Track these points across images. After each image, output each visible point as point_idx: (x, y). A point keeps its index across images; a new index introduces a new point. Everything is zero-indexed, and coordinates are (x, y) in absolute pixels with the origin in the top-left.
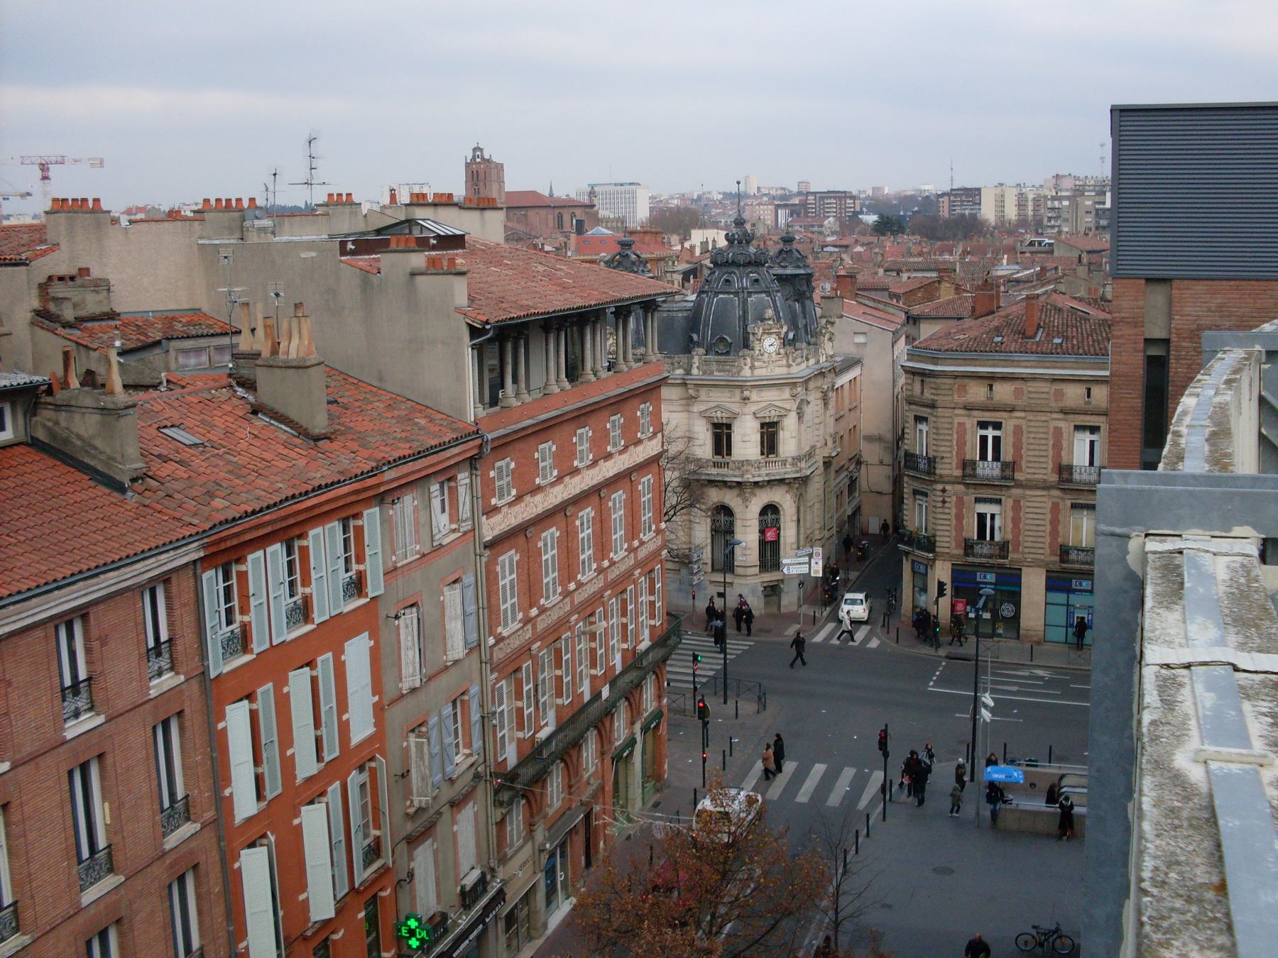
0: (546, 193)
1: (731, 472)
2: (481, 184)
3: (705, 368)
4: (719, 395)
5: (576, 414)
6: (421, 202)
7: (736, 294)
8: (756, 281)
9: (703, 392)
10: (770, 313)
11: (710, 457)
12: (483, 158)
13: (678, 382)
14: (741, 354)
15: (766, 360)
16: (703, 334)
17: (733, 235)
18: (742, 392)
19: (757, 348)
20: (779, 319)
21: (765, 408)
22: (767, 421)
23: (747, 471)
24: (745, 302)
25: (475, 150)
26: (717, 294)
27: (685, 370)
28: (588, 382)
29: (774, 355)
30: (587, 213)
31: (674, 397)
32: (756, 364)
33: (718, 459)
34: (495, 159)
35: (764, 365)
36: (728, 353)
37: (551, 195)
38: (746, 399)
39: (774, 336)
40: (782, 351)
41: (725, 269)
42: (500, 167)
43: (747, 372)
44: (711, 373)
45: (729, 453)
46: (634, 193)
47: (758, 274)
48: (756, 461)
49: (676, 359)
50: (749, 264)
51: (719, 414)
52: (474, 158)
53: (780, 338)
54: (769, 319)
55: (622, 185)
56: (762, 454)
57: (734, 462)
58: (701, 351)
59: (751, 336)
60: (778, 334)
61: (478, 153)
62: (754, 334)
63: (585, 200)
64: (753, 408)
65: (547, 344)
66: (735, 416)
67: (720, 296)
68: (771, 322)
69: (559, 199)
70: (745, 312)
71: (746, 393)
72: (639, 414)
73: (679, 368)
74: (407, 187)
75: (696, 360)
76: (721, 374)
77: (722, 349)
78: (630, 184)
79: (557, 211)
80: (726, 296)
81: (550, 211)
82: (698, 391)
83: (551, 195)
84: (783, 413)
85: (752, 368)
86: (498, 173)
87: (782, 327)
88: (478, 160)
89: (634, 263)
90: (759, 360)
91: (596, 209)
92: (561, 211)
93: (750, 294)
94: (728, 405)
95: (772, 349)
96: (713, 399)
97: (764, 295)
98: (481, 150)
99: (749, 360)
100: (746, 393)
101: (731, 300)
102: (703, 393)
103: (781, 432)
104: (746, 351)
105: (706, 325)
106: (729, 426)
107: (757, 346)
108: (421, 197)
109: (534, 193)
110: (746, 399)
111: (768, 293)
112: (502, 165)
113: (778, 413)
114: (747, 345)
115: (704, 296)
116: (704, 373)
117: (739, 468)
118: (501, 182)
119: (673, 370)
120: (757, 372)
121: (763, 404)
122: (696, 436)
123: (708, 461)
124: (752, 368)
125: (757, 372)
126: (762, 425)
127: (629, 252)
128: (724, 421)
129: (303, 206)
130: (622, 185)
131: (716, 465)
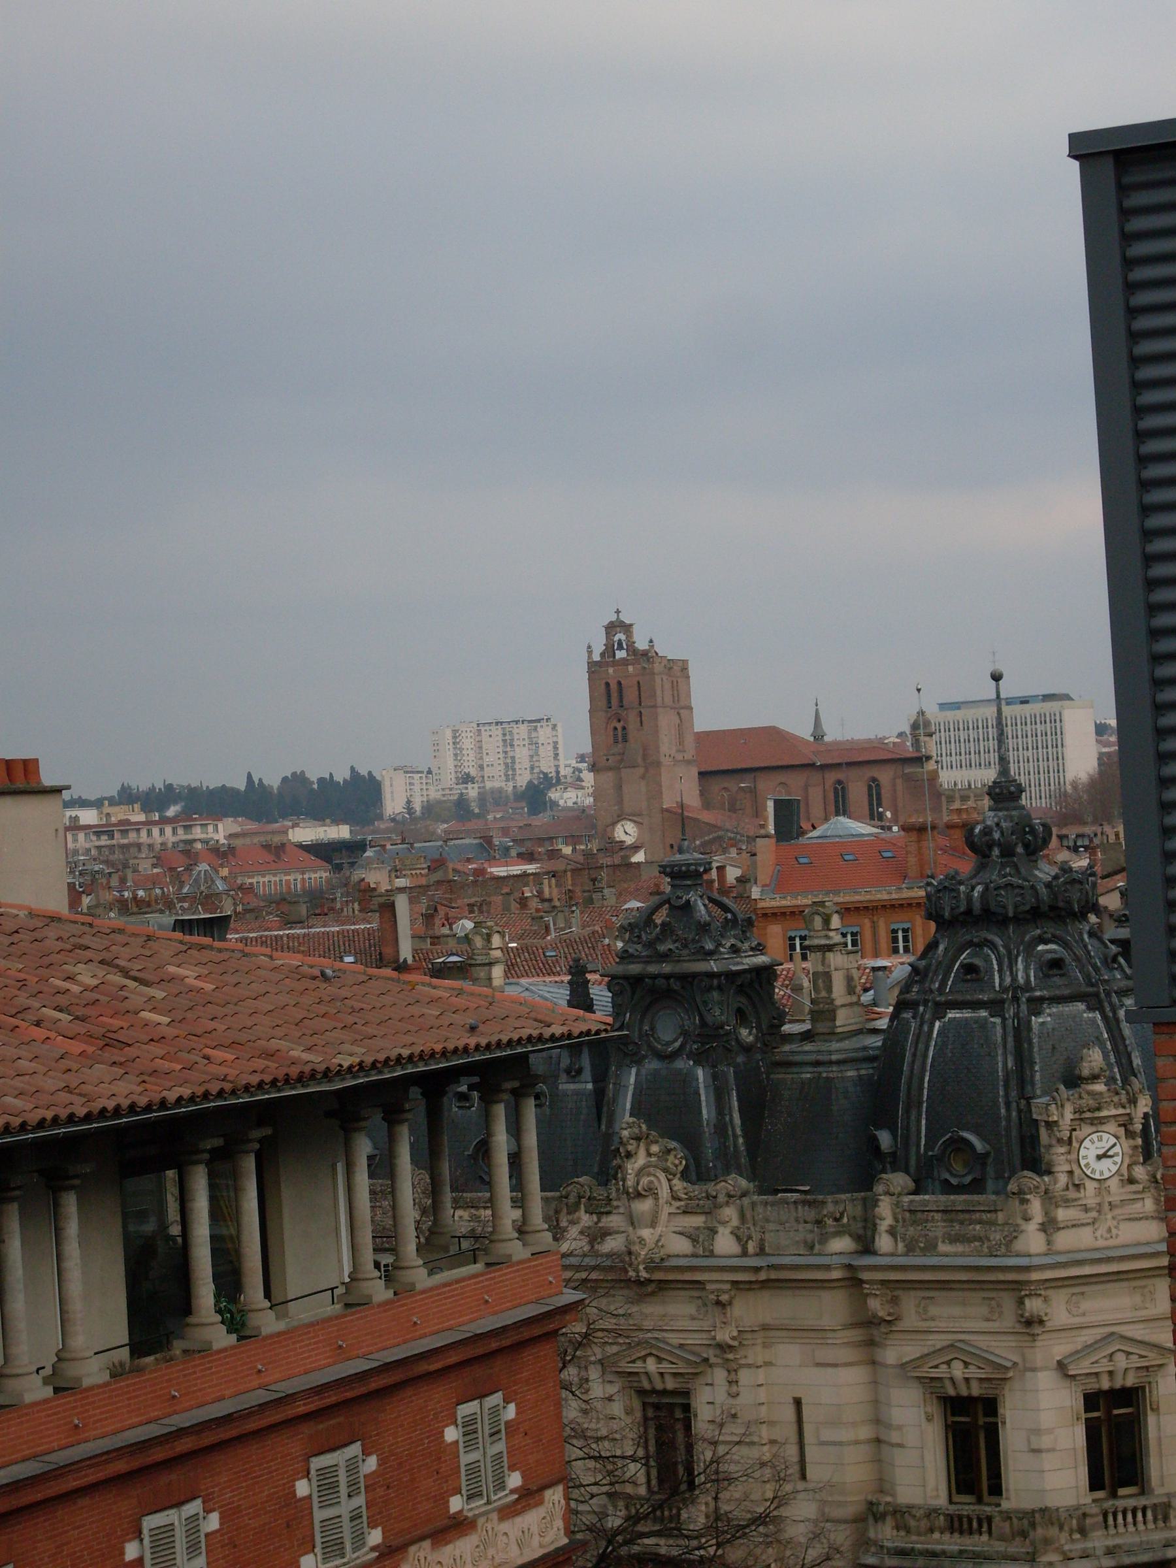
0: (805, 732)
1: (1000, 1546)
2: (632, 718)
3: (911, 1231)
4: (957, 1311)
5: (121, 1466)
6: (20, 784)
7: (996, 1006)
8: (1056, 964)
9: (909, 1303)
10: (1094, 1059)
11: (942, 1500)
12: (632, 649)
13: (836, 1274)
14: (1012, 1187)
15: (1091, 1202)
16: (907, 1128)
17: (987, 831)
18: (1021, 1302)
19: (1062, 1167)
20: (1128, 1071)
21: (1089, 1348)
22: (1105, 1385)
23: (1047, 1541)
24: (1021, 1034)
25: (611, 628)
26: (940, 1009)
27: (857, 1238)
28: (204, 1351)
29: (1114, 1184)
30: (908, 778)
31: (826, 1322)
32: (1062, 1214)
33: (967, 1506)
34: (667, 649)
35: (1085, 1217)
36: (976, 1186)
37: (818, 736)
38: (1031, 1323)
39: (1112, 1127)
40: (1140, 1172)
41: (964, 936)
42: (679, 670)
43: (1032, 1241)
44: (931, 1248)
45: (996, 1489)
46: (1056, 721)
47: (1065, 945)
48: (1071, 1511)
49: (830, 1207)
50: (1035, 914)
51: (958, 1371)
52: (609, 650)
53: (1130, 1134)
54: (1094, 1078)
55: (1024, 701)
56: (1095, 1484)
57: (1007, 1516)
58: (899, 1180)
59: (1043, 1132)
60: (1126, 1124)
61: (621, 636)
62: (1050, 1125)
63: (909, 749)
64: (1060, 1349)
65: (58, 1232)
66: (1000, 1376)
67: (952, 1014)
68: (1100, 1087)
69: (836, 745)
70: (1023, 1058)
71: (1033, 1306)
72: (451, 1434)
73: (838, 1234)
74: (497, 731)
75: (885, 1210)
76: (959, 1248)
77: (959, 1172)
78: (1047, 698)
79: (832, 777)
80: (967, 1014)
81: (816, 777)
82: (895, 1301)
83: (818, 736)
84: (1153, 1358)
85: (1049, 1226)
86: (674, 686)
87: (1133, 1101)
88: (621, 654)
89: (704, 928)
90: (1067, 1203)
91: (931, 766)
92: (840, 775)
93: (1037, 1006)
94: (981, 1341)
95: (1107, 1168)
96: (942, 1325)
97: (1081, 1006)
98: (627, 628)
99: (1036, 1207)
100: (1033, 1306)
101: (983, 1024)
102: (910, 1309)
103: (1151, 1419)
104: (1029, 1179)
105: (913, 1103)
106: (991, 1405)
107: (1059, 1156)
108: (19, 772)
109: (772, 735)
110: (1031, 1323)
111: (1094, 1001)
112: (684, 666)
113: (1135, 1362)
114: (1036, 1163)
115: (907, 1015)
116: (910, 1249)
117: (1024, 1534)
118: (682, 708)
119: (824, 1239)
120: (1064, 1240)
121: (1088, 1337)
122: (895, 1437)
123: (931, 1513)
124: (1049, 1226)
125: (1064, 1240)
126: (1091, 1401)
127: (692, 896)
128: (976, 1391)
129: (241, 785)
130: (1024, 701)
131: (957, 1525)
